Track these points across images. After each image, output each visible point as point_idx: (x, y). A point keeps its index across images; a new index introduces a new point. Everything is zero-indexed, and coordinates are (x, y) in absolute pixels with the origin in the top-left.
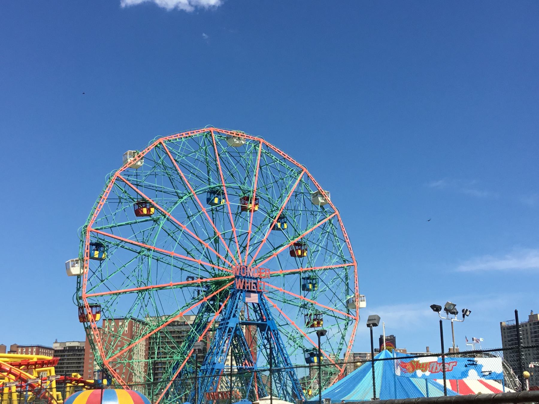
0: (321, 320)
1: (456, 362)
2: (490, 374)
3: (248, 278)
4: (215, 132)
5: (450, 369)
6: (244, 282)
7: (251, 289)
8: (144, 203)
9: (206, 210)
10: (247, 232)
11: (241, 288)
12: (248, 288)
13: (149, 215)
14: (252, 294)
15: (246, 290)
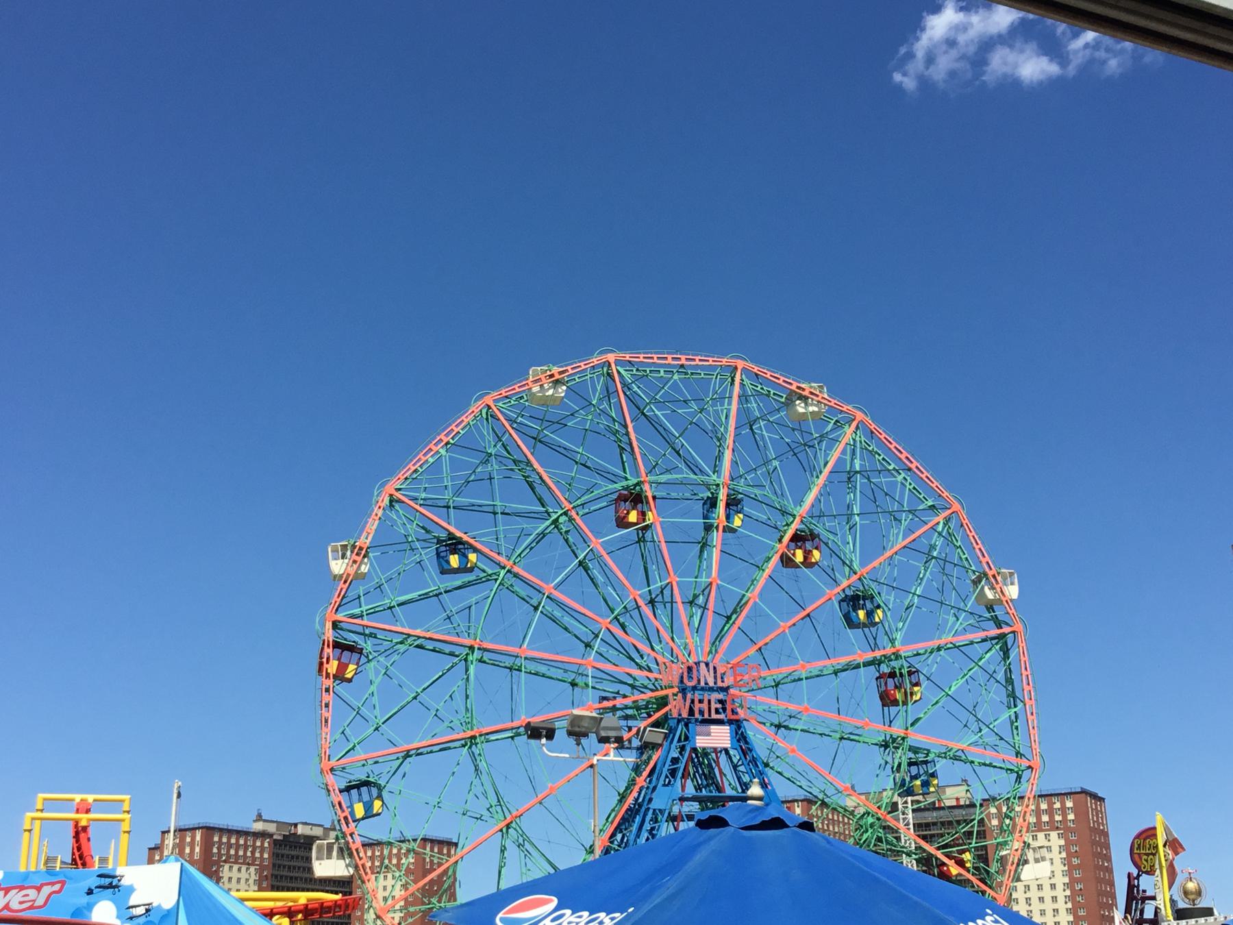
0: (933, 775)
1: (63, 883)
2: (147, 911)
3: (703, 689)
4: (617, 362)
5: (40, 902)
6: (693, 701)
7: (710, 715)
8: (455, 545)
9: (604, 544)
10: (668, 584)
11: (685, 715)
12: (702, 713)
13: (464, 569)
14: (714, 728)
15: (697, 720)
